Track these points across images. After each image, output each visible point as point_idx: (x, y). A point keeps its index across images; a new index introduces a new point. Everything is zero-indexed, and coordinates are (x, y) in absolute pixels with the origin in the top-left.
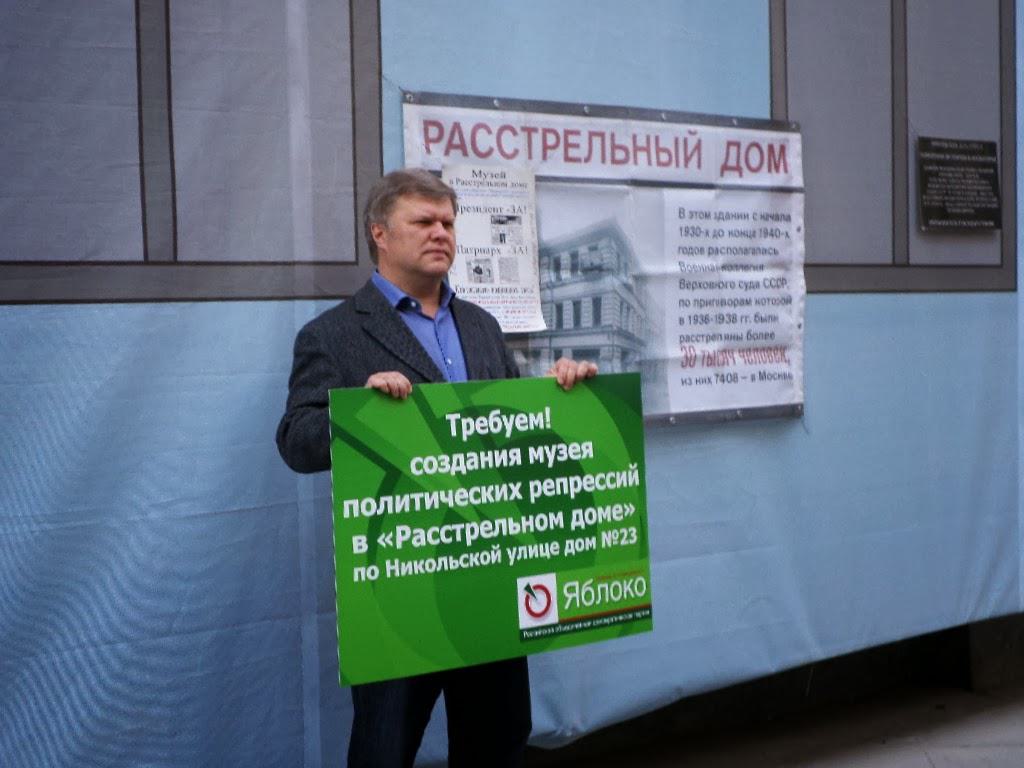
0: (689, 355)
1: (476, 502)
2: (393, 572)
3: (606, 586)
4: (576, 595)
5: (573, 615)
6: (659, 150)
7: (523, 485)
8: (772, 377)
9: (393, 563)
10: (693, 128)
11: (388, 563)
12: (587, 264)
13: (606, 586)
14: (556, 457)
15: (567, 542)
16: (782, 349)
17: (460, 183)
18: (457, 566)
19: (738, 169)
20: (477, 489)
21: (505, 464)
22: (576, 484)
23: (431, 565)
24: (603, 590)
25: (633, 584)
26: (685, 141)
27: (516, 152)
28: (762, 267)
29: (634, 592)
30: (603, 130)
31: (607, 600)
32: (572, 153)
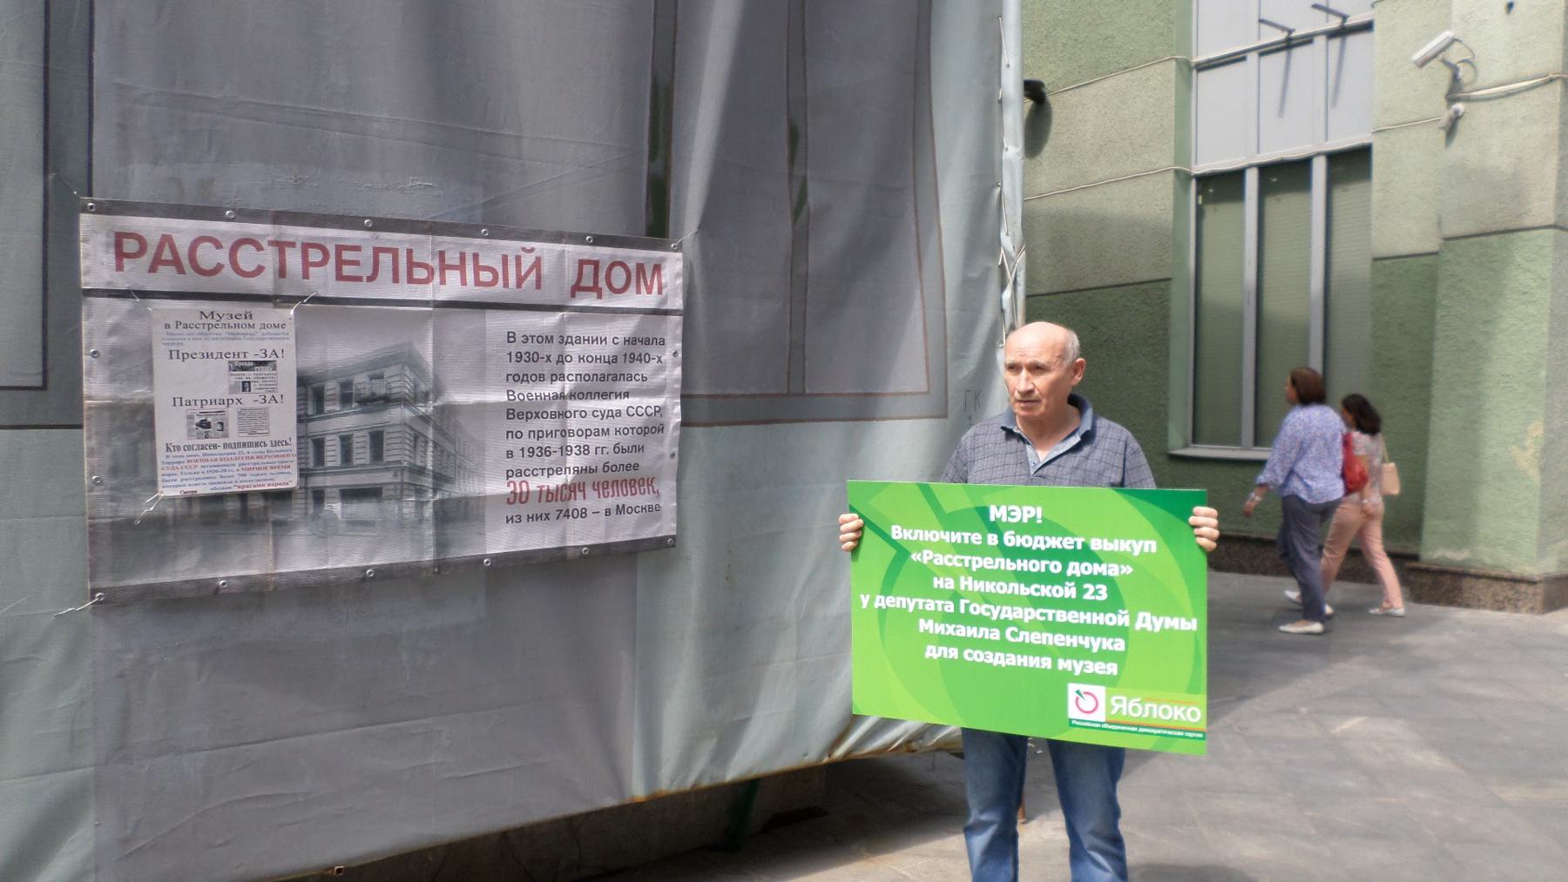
0: (518, 491)
6: (478, 269)
7: (1082, 596)
8: (633, 510)
10: (529, 245)
12: (366, 393)
16: (650, 481)
17: (181, 327)
19: (595, 288)
22: (1029, 614)
26: (518, 259)
27: (260, 269)
28: (627, 395)
30: (407, 286)
32: (347, 270)
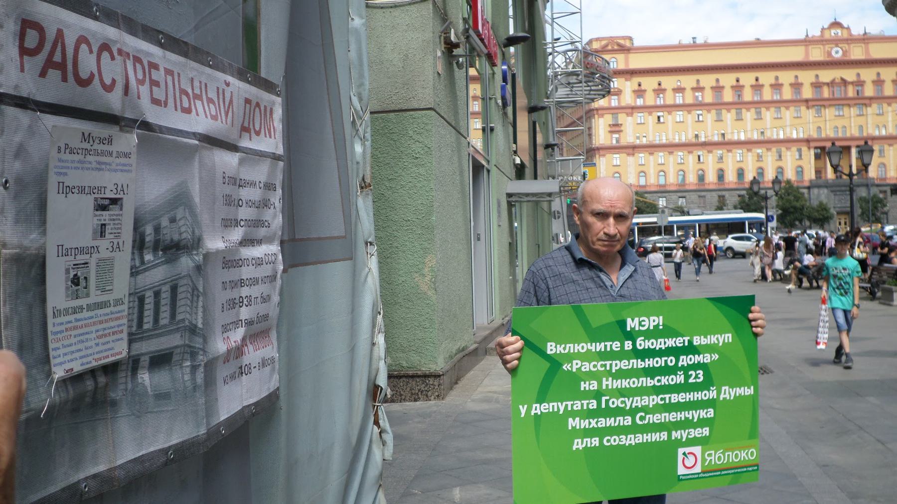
1: (659, 384)
2: (607, 385)
3: (731, 453)
4: (713, 458)
5: (708, 469)
9: (607, 380)
11: (604, 379)
13: (731, 453)
14: (687, 436)
15: (723, 388)
18: (652, 384)
20: (659, 378)
21: (658, 440)
23: (634, 383)
24: (728, 455)
25: (748, 452)
29: (748, 457)
31: (731, 461)
